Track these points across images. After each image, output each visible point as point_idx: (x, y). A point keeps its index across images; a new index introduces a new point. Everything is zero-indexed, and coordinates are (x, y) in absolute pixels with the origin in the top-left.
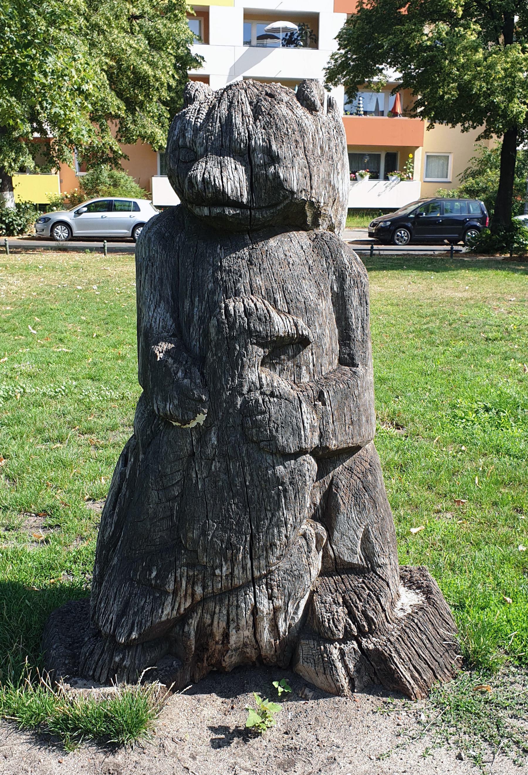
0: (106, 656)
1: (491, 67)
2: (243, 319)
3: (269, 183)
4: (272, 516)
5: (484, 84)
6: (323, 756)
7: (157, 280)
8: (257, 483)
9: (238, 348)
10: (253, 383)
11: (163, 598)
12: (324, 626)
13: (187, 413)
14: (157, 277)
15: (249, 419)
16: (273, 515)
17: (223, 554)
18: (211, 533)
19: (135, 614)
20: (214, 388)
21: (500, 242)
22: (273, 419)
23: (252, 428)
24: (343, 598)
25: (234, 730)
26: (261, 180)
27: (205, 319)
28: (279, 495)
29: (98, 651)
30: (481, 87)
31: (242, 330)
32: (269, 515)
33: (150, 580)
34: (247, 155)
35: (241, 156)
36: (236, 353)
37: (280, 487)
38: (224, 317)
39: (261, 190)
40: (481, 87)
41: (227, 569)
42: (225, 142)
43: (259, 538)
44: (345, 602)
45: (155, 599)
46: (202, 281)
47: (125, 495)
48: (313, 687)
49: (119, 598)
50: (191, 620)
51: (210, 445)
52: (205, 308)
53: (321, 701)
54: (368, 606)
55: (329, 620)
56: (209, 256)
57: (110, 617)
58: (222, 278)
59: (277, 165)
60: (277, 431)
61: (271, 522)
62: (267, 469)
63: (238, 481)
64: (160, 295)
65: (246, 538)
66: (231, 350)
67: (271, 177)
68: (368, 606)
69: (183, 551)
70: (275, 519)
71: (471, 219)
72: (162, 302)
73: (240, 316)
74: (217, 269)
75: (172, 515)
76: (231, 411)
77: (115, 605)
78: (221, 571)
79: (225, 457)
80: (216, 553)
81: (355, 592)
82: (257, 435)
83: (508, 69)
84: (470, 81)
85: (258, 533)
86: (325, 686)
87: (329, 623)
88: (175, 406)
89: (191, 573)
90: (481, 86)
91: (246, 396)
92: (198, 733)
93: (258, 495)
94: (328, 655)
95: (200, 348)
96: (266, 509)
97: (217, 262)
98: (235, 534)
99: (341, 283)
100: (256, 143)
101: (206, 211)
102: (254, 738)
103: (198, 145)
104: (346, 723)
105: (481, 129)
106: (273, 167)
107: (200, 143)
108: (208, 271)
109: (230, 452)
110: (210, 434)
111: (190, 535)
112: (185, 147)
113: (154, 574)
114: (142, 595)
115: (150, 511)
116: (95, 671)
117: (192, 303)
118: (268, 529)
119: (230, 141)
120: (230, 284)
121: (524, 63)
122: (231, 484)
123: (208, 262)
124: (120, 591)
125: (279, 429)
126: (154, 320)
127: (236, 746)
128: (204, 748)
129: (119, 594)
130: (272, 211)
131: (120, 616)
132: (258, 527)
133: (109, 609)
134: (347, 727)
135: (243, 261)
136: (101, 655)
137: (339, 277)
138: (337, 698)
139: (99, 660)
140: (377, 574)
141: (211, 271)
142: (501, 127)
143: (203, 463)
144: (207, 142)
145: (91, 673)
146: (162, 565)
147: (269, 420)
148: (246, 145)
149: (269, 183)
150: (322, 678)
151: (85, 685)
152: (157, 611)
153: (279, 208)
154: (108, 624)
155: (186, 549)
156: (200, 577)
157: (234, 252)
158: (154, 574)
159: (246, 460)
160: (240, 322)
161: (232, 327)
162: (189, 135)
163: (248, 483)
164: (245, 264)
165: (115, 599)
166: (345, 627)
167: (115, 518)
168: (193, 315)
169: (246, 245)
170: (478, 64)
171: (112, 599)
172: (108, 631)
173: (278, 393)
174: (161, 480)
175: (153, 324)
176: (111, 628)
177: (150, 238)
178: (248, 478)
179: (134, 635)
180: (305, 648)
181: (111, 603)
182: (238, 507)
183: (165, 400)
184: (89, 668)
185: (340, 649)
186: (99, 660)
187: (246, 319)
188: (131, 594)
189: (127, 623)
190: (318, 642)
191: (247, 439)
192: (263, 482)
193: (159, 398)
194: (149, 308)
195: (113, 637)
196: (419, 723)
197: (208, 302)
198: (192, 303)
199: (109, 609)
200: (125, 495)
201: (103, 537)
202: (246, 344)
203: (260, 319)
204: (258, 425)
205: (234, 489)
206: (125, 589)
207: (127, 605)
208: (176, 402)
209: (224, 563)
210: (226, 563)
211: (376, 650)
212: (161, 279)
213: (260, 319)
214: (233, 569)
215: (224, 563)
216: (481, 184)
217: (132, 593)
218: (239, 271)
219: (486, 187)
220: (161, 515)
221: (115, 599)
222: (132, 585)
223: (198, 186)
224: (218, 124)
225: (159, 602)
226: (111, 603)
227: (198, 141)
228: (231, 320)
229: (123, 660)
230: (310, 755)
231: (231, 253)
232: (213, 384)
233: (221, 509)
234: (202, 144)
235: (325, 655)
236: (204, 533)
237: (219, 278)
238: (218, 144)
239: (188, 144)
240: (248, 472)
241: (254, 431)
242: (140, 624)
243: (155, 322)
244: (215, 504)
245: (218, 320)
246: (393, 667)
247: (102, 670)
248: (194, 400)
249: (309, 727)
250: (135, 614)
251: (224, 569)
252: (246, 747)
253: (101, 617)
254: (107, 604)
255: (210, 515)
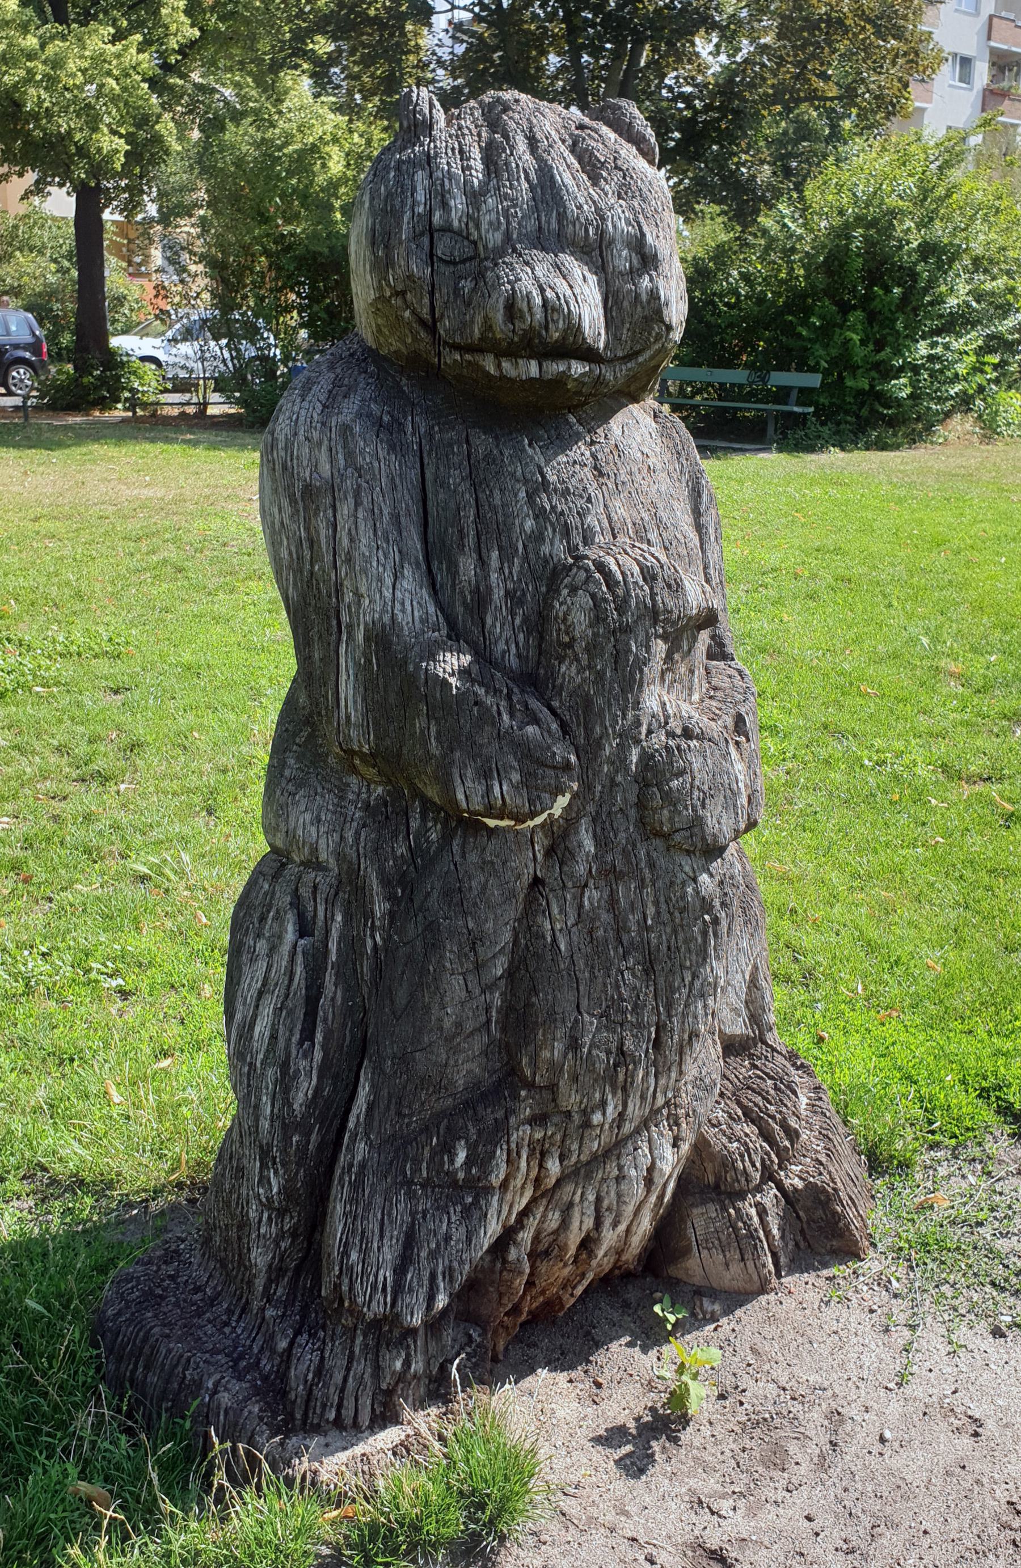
0: (362, 1367)
1: (57, 63)
2: (641, 588)
3: (639, 309)
4: (693, 979)
5: (44, 95)
6: (817, 1415)
7: (386, 518)
8: (665, 917)
9: (634, 649)
10: (653, 716)
11: (483, 1202)
12: (735, 1169)
13: (539, 797)
14: (386, 512)
15: (655, 789)
16: (695, 976)
17: (610, 1078)
18: (587, 1040)
19: (433, 1255)
20: (588, 735)
21: (96, 388)
22: (697, 783)
23: (662, 808)
24: (739, 1103)
25: (637, 1428)
26: (626, 304)
27: (524, 594)
28: (705, 934)
29: (337, 1364)
30: (40, 102)
31: (643, 611)
32: (688, 978)
33: (452, 1174)
34: (597, 252)
35: (585, 253)
36: (631, 659)
37: (707, 917)
38: (604, 589)
39: (623, 323)
40: (40, 102)
41: (615, 1107)
42: (549, 223)
43: (672, 1029)
44: (747, 1113)
45: (466, 1212)
46: (506, 515)
47: (333, 999)
48: (714, 1293)
49: (391, 1231)
50: (521, 1235)
51: (581, 857)
52: (520, 572)
53: (739, 1313)
54: (784, 1109)
55: (742, 1156)
56: (512, 463)
57: (381, 1278)
58: (553, 508)
59: (654, 273)
60: (703, 807)
61: (690, 991)
62: (684, 884)
63: (633, 919)
64: (400, 552)
65: (650, 1033)
66: (619, 656)
67: (644, 297)
68: (784, 1109)
69: (523, 1093)
70: (697, 984)
71: (16, 346)
72: (406, 565)
73: (636, 583)
74: (537, 489)
75: (488, 1021)
76: (619, 778)
77: (386, 1249)
78: (604, 1114)
79: (610, 875)
80: (596, 1080)
81: (753, 1090)
82: (671, 820)
83: (86, 70)
84: (15, 86)
85: (669, 1016)
86: (738, 1285)
87: (743, 1161)
88: (515, 787)
89: (539, 1135)
90: (39, 97)
91: (644, 744)
92: (585, 1461)
93: (668, 941)
94: (745, 1223)
95: (519, 656)
96: (682, 967)
97: (534, 474)
98: (631, 1031)
99: (696, 501)
100: (614, 227)
101: (533, 369)
102: (684, 1429)
103: (484, 226)
104: (800, 1340)
105: (31, 177)
106: (647, 278)
107: (491, 223)
108: (516, 495)
109: (619, 865)
110: (577, 833)
111: (546, 1054)
112: (447, 228)
113: (461, 1156)
114: (438, 1209)
115: (447, 1023)
116: (340, 1407)
117: (482, 562)
118: (687, 1005)
119: (559, 222)
120: (573, 520)
121: (114, 62)
122: (620, 928)
123: (513, 475)
124: (390, 1214)
125: (707, 801)
126: (398, 606)
127: (664, 1457)
128: (621, 1485)
129: (391, 1222)
130: (629, 365)
131: (400, 1271)
132: (669, 1006)
133: (374, 1260)
134: (808, 1345)
135: (586, 469)
136: (348, 1369)
137: (693, 490)
138: (763, 1299)
139: (345, 1380)
140: (768, 1045)
141: (522, 494)
142: (83, 176)
143: (568, 897)
144: (508, 223)
145: (332, 1415)
146: (479, 1133)
147: (692, 786)
148: (597, 229)
149: (639, 309)
150: (736, 1268)
151: (327, 1445)
152: (478, 1233)
153: (641, 359)
154: (379, 1296)
155: (531, 1086)
156: (558, 1137)
157: (563, 452)
158: (461, 1156)
159: (647, 875)
160: (637, 596)
161: (622, 606)
162: (458, 204)
163: (649, 922)
164: (590, 476)
165: (382, 1236)
166: (763, 1160)
167: (318, 1055)
168: (489, 589)
169: (578, 437)
170: (31, 56)
171: (376, 1238)
172: (382, 1310)
173: (698, 731)
174: (473, 948)
175: (400, 616)
176: (385, 1303)
177: (345, 430)
178: (651, 910)
179: (442, 1301)
180: (699, 1223)
181: (375, 1245)
182: (634, 975)
183: (485, 775)
184: (324, 1406)
185: (758, 1205)
186: (345, 1380)
187: (646, 588)
188: (413, 1214)
189: (420, 1280)
190: (722, 1203)
191: (649, 830)
192: (677, 914)
193: (469, 772)
194: (380, 579)
195: (393, 1319)
196: (896, 1296)
197: (526, 558)
198: (482, 562)
199: (374, 1260)
200: (333, 999)
201: (287, 1103)
202: (648, 639)
203: (669, 586)
204: (670, 799)
205: (625, 938)
206: (401, 1207)
207: (410, 1242)
208: (516, 777)
209: (610, 1097)
210: (614, 1094)
211: (809, 1186)
212: (396, 518)
213: (669, 586)
214: (625, 1105)
215: (610, 1097)
216: (8, 280)
217: (417, 1212)
218: (585, 489)
219: (19, 286)
220: (469, 1026)
221: (382, 1236)
222: (411, 1195)
223: (532, 315)
224: (525, 185)
225: (476, 1214)
226: (375, 1245)
227: (485, 220)
228: (620, 592)
229: (407, 1364)
230: (796, 1423)
231: (556, 455)
232: (586, 728)
233: (605, 985)
234: (495, 226)
235: (740, 1224)
236: (574, 1044)
237: (548, 508)
238: (531, 225)
239: (456, 223)
240: (651, 899)
241: (665, 812)
242: (450, 1273)
243: (403, 611)
244: (593, 978)
245: (593, 596)
246: (839, 1209)
247: (357, 1400)
248: (554, 768)
249: (750, 1370)
250: (433, 1255)
251: (610, 1109)
252: (683, 1451)
253: (358, 1285)
254: (365, 1252)
255: (584, 1003)
